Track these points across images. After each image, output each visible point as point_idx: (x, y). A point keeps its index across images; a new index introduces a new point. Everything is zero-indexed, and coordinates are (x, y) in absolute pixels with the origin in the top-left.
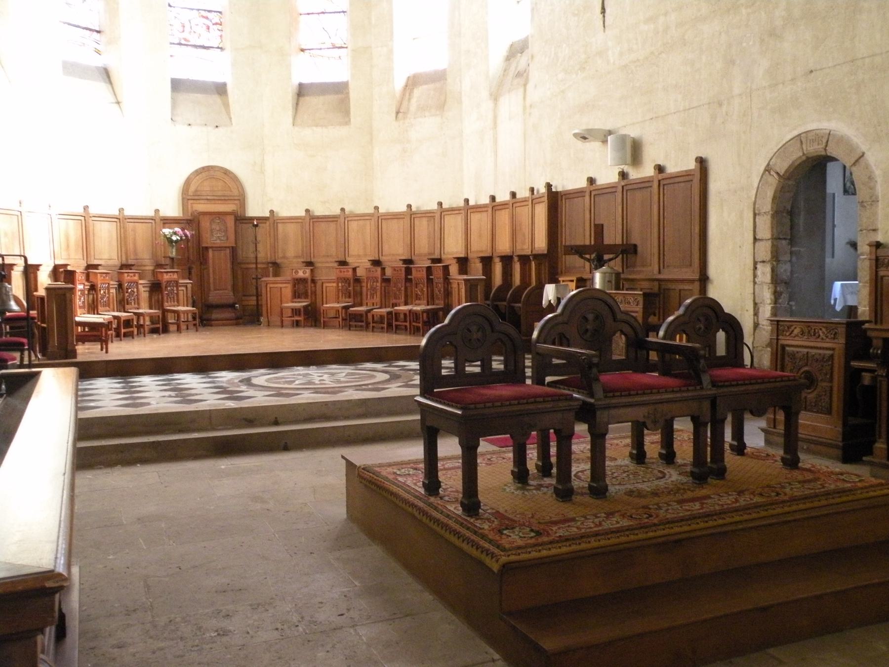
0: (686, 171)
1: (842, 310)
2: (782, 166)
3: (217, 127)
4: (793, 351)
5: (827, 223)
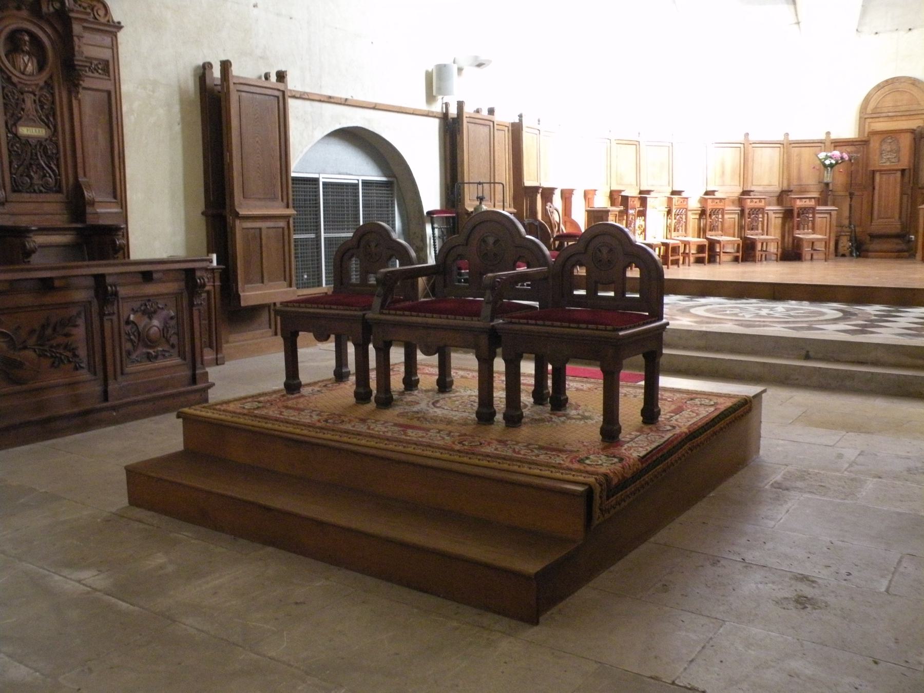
3: (910, 29)
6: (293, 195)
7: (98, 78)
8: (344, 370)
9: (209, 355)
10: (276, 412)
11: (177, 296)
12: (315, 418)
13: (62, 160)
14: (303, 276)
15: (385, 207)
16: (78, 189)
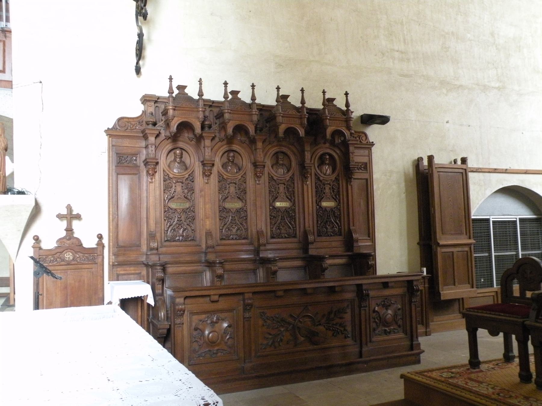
6: (473, 230)
7: (361, 173)
8: (510, 355)
9: (421, 329)
10: (463, 382)
11: (402, 296)
12: (491, 390)
13: (342, 218)
14: (480, 280)
15: (536, 235)
16: (350, 233)
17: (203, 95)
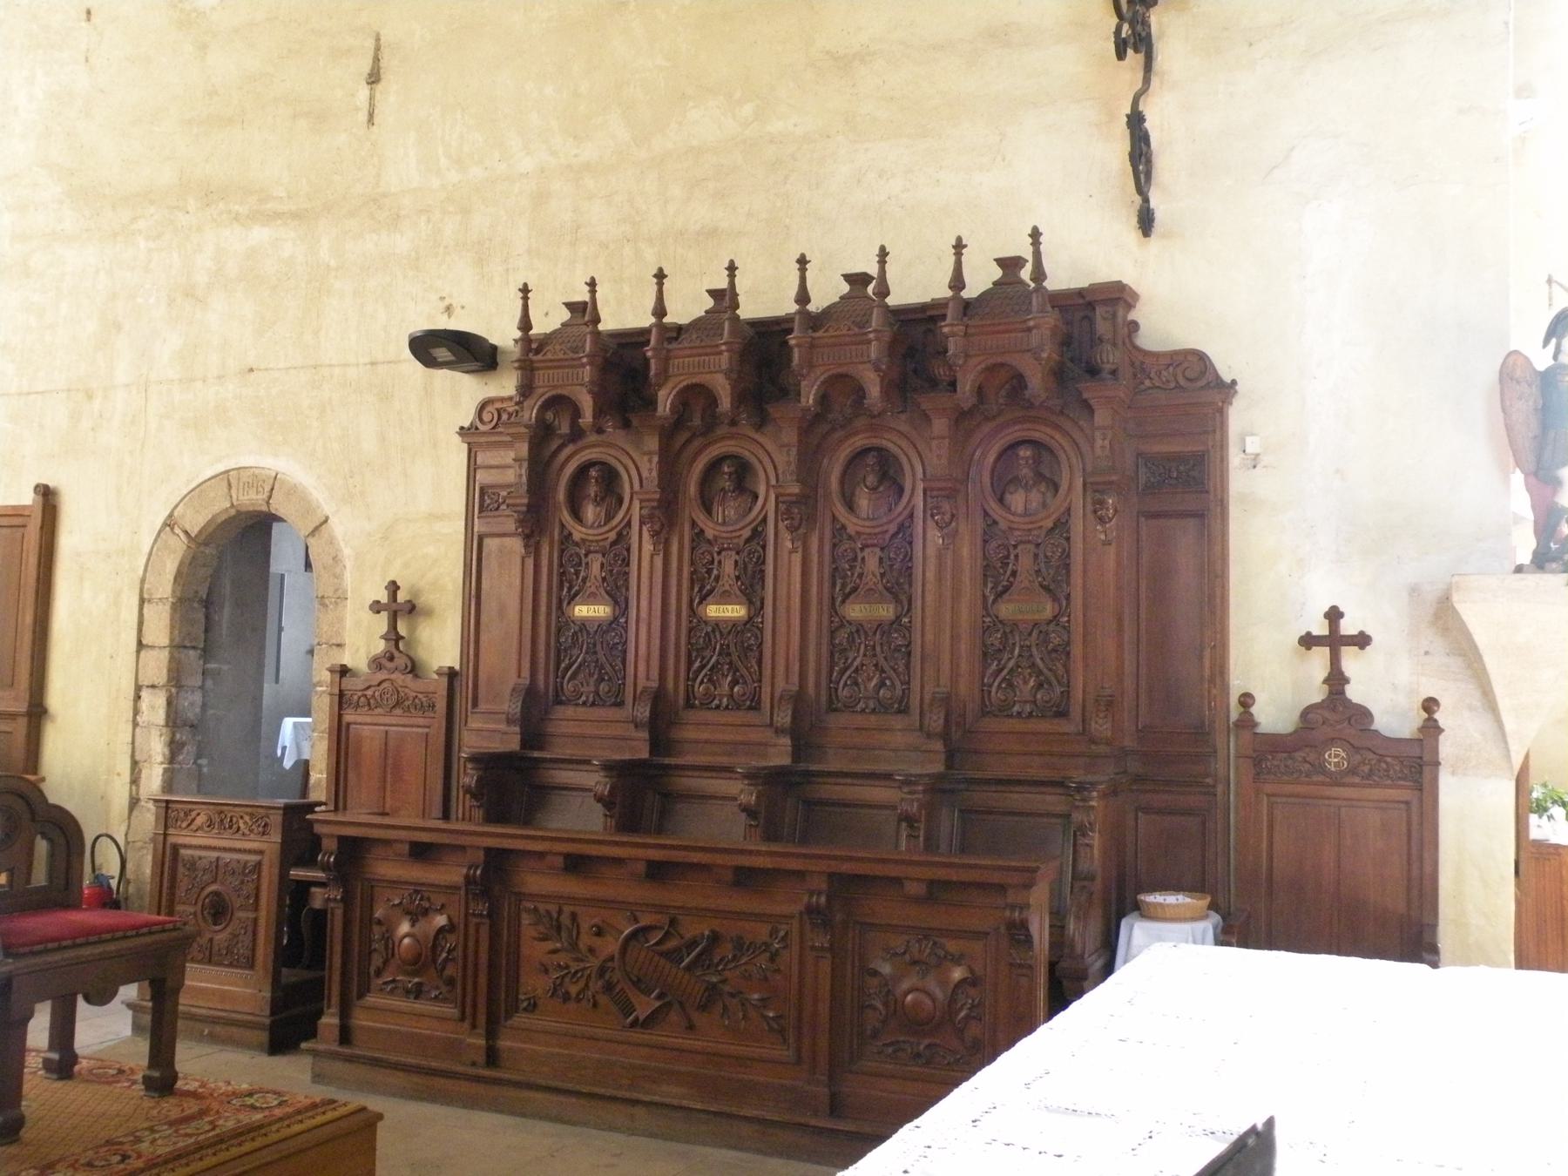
0: (14, 507)
1: (293, 767)
2: (196, 521)
4: (192, 857)
5: (269, 626)
17: (665, 314)
